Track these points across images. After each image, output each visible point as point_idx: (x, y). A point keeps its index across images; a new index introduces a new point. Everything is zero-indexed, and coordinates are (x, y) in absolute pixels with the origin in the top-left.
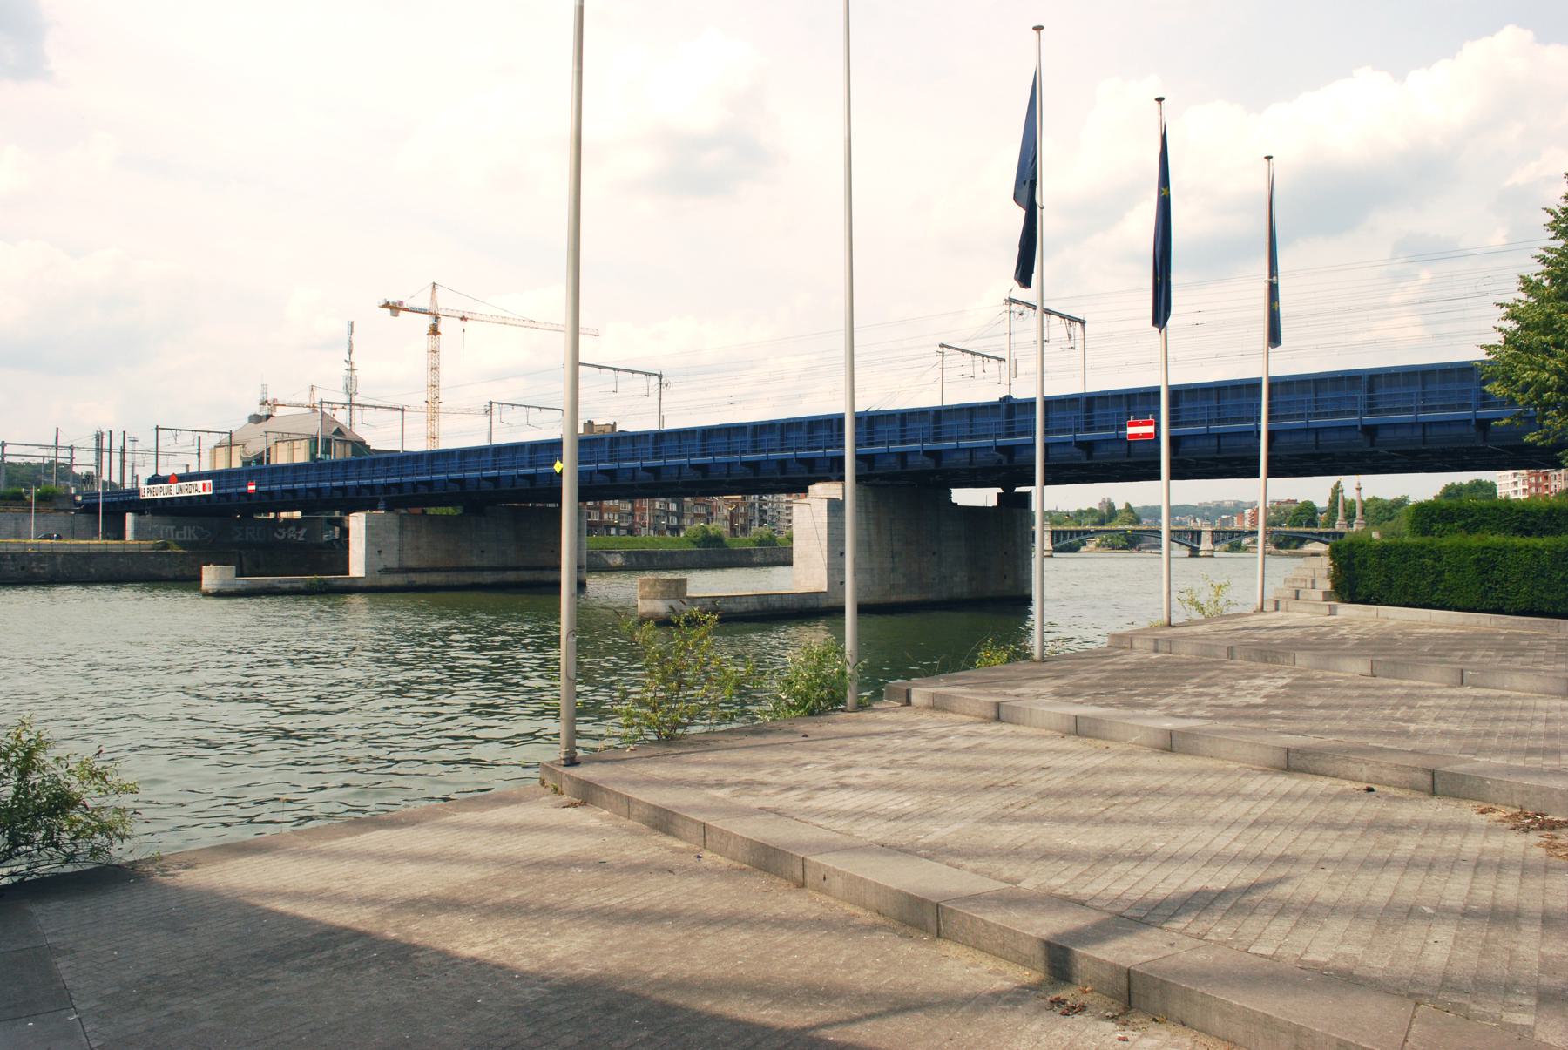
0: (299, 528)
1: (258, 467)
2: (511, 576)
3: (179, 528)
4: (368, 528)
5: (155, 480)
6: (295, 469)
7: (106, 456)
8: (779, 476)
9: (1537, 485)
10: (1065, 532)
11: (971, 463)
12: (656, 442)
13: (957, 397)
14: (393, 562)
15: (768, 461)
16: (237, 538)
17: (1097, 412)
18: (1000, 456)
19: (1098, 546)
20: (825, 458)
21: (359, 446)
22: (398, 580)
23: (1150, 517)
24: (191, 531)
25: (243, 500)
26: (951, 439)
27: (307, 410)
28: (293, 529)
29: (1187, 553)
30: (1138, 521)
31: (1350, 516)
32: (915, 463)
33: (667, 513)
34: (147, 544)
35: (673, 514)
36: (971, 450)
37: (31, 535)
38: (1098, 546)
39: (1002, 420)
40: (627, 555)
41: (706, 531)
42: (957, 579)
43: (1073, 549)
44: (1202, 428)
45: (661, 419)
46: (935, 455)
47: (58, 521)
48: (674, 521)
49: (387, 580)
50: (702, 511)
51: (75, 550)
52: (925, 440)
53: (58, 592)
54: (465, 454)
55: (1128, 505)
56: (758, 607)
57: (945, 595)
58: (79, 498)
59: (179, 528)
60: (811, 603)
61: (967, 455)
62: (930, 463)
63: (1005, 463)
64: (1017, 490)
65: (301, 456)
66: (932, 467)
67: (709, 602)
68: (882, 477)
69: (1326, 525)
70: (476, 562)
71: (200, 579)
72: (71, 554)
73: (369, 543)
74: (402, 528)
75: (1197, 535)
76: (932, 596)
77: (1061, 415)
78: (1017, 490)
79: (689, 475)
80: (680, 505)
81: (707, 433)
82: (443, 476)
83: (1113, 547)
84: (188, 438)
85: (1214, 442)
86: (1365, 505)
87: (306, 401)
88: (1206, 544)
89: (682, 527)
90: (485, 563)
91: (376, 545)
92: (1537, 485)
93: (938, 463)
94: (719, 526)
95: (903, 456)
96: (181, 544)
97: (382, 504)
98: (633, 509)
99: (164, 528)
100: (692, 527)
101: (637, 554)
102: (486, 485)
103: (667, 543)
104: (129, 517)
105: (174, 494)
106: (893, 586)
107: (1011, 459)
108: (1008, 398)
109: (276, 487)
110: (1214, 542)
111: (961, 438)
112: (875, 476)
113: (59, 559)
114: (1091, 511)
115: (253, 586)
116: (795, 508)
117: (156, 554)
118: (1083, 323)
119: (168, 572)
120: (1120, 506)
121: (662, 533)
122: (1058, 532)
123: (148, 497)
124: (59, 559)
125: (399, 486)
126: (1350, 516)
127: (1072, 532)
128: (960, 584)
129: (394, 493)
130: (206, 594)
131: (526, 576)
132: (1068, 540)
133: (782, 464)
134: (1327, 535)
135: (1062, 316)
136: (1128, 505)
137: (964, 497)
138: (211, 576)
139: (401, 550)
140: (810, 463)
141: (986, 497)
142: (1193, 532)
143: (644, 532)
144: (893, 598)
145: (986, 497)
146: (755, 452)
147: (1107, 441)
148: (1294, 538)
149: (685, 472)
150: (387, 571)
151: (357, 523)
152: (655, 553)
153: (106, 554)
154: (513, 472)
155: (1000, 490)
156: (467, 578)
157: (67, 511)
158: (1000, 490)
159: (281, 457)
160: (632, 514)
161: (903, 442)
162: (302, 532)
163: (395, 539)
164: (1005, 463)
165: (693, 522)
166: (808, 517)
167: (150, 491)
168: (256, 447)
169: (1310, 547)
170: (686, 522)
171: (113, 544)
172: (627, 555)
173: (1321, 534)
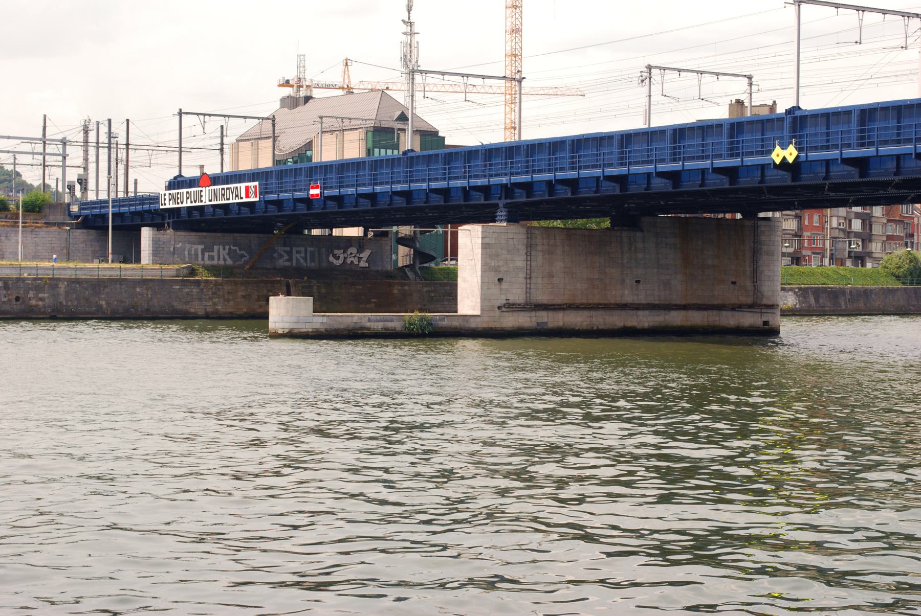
0: (361, 249)
1: (298, 166)
2: (676, 318)
3: (208, 248)
4: (485, 246)
5: (177, 183)
6: (343, 167)
7: (92, 151)
12: (862, 122)
14: (517, 295)
15: (879, 158)
16: (282, 263)
21: (430, 137)
22: (524, 320)
24: (224, 253)
25: (302, 209)
27: (340, 92)
28: (353, 250)
33: (848, 233)
34: (170, 270)
35: (857, 235)
37: (26, 256)
40: (803, 293)
45: (516, 127)
47: (50, 237)
48: (856, 246)
49: (511, 321)
50: (899, 231)
51: (81, 275)
53: (81, 327)
54: (554, 146)
58: (75, 209)
59: (208, 248)
65: (353, 148)
70: (629, 297)
71: (265, 316)
72: (77, 281)
73: (486, 268)
74: (530, 247)
79: (840, 173)
80: (867, 221)
81: (868, 115)
82: (424, 186)
84: (214, 125)
87: (338, 80)
89: (870, 255)
90: (642, 299)
91: (496, 270)
96: (213, 270)
97: (502, 213)
98: (801, 228)
99: (189, 246)
101: (817, 292)
102: (659, 184)
103: (851, 277)
104: (146, 233)
105: (206, 201)
109: (350, 191)
113: (62, 287)
115: (336, 326)
117: (184, 283)
119: (196, 307)
121: (842, 263)
123: (170, 205)
124: (62, 287)
125: (527, 187)
129: (520, 197)
130: (276, 336)
131: (697, 318)
138: (283, 310)
139: (529, 277)
149: (836, 170)
150: (510, 307)
151: (470, 238)
152: (842, 292)
153: (120, 281)
154: (597, 172)
156: (617, 320)
157: (60, 225)
159: (327, 152)
160: (798, 235)
162: (365, 255)
163: (520, 262)
167: (173, 198)
168: (290, 142)
171: (128, 270)
172: (803, 293)
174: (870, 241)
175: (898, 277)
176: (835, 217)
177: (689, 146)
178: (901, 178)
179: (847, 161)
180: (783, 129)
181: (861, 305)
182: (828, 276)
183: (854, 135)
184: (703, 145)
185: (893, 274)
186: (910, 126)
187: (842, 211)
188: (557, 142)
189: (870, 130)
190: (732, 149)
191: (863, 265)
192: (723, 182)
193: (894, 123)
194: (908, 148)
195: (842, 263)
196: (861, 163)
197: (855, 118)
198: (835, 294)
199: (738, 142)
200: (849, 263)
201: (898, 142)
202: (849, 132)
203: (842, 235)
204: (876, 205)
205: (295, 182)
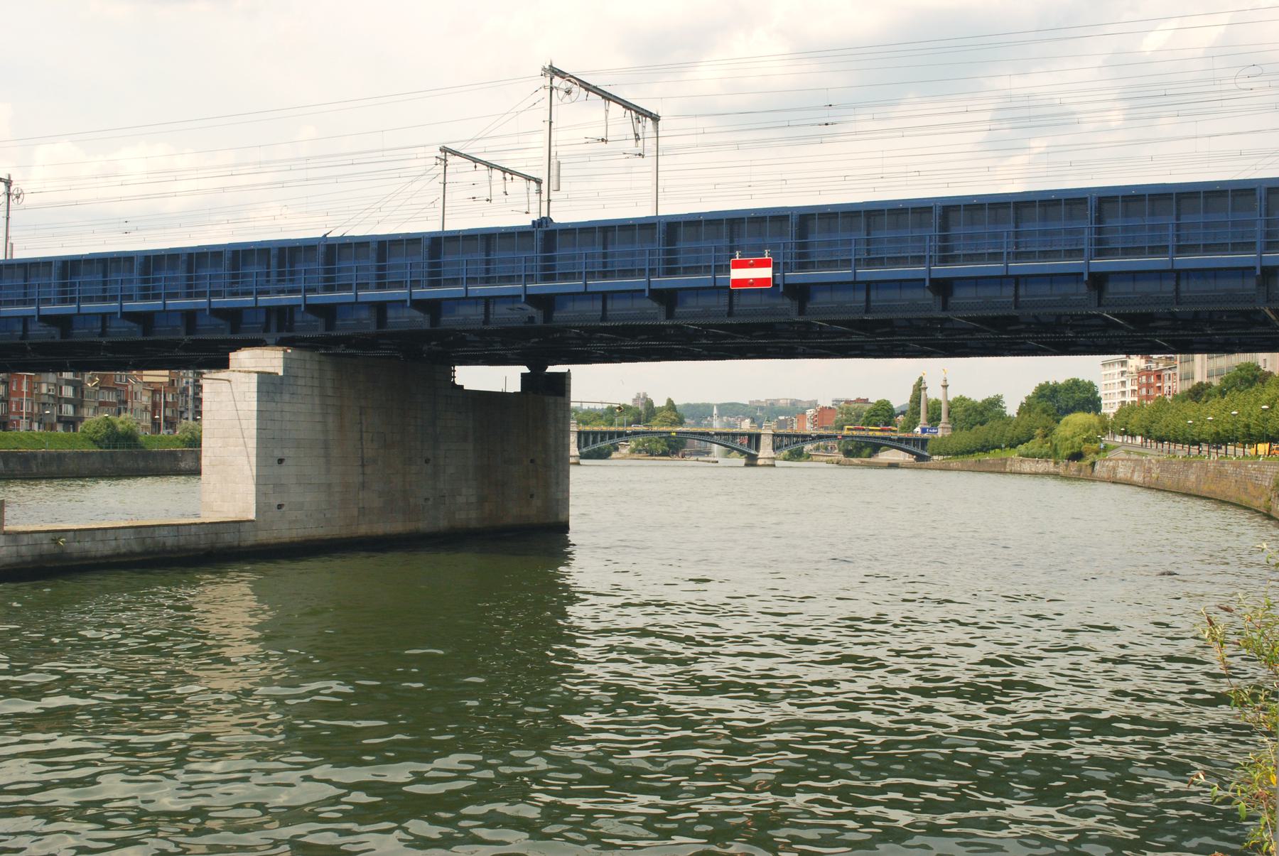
8: (186, 338)
9: (1149, 386)
10: (595, 434)
11: (486, 322)
13: (467, 216)
15: (166, 313)
17: (681, 245)
18: (531, 310)
19: (633, 451)
20: (256, 309)
23: (692, 417)
26: (455, 282)
29: (743, 461)
30: (681, 423)
31: (934, 419)
32: (401, 319)
33: (59, 400)
35: (68, 401)
36: (488, 301)
38: (633, 451)
39: (537, 253)
41: (111, 425)
42: (461, 500)
43: (602, 455)
44: (844, 273)
46: (432, 307)
48: (68, 410)
50: (111, 397)
52: (416, 283)
55: (670, 402)
56: (136, 548)
57: (443, 524)
60: (229, 538)
61: (481, 309)
62: (421, 320)
63: (539, 321)
64: (551, 369)
66: (427, 326)
67: (46, 540)
68: (347, 341)
69: (903, 429)
75: (755, 439)
76: (423, 525)
77: (628, 248)
78: (551, 369)
79: (39, 332)
80: (78, 387)
83: (651, 453)
85: (861, 296)
86: (951, 406)
88: (766, 451)
92: (1149, 386)
93: (435, 320)
94: (134, 420)
95: (380, 308)
100: (92, 419)
103: (59, 441)
106: (362, 511)
107: (548, 317)
108: (543, 222)
110: (776, 448)
111: (473, 281)
112: (337, 341)
114: (623, 409)
116: (207, 386)
118: (656, 119)
120: (659, 402)
122: (587, 434)
126: (934, 419)
127: (603, 434)
128: (465, 507)
132: (599, 445)
133: (190, 317)
134: (908, 441)
135: (627, 105)
136: (670, 402)
137: (471, 377)
140: (233, 316)
141: (505, 378)
142: (750, 436)
143: (24, 424)
144: (363, 530)
145: (505, 378)
146: (145, 297)
147: (698, 291)
148: (867, 445)
149: (116, 326)
152: (34, 456)
155: (525, 369)
158: (525, 369)
161: (380, 286)
164: (539, 321)
165: (96, 410)
166: (231, 400)
169: (887, 456)
170: (87, 412)
173: (900, 440)
174: (82, 406)
175: (95, 442)
176: (47, 383)
177: (85, 283)
178: (108, 339)
179: (45, 319)
180: (50, 275)
181: (54, 468)
182: (22, 440)
183: (136, 285)
184: (25, 287)
185: (91, 439)
186: (116, 281)
187: (52, 377)
188: (384, 242)
189: (155, 280)
190: (64, 293)
191: (75, 430)
192: (54, 334)
193: (599, 250)
194: (114, 306)
195: (53, 427)
196: (62, 322)
197: (226, 262)
198: (26, 459)
199: (73, 284)
200: (60, 428)
201: (104, 299)
202: (131, 281)
203: (51, 401)
204: (1136, 353)
205: (105, 283)
